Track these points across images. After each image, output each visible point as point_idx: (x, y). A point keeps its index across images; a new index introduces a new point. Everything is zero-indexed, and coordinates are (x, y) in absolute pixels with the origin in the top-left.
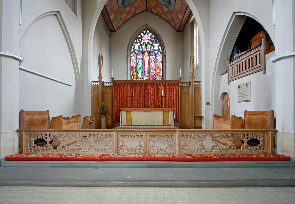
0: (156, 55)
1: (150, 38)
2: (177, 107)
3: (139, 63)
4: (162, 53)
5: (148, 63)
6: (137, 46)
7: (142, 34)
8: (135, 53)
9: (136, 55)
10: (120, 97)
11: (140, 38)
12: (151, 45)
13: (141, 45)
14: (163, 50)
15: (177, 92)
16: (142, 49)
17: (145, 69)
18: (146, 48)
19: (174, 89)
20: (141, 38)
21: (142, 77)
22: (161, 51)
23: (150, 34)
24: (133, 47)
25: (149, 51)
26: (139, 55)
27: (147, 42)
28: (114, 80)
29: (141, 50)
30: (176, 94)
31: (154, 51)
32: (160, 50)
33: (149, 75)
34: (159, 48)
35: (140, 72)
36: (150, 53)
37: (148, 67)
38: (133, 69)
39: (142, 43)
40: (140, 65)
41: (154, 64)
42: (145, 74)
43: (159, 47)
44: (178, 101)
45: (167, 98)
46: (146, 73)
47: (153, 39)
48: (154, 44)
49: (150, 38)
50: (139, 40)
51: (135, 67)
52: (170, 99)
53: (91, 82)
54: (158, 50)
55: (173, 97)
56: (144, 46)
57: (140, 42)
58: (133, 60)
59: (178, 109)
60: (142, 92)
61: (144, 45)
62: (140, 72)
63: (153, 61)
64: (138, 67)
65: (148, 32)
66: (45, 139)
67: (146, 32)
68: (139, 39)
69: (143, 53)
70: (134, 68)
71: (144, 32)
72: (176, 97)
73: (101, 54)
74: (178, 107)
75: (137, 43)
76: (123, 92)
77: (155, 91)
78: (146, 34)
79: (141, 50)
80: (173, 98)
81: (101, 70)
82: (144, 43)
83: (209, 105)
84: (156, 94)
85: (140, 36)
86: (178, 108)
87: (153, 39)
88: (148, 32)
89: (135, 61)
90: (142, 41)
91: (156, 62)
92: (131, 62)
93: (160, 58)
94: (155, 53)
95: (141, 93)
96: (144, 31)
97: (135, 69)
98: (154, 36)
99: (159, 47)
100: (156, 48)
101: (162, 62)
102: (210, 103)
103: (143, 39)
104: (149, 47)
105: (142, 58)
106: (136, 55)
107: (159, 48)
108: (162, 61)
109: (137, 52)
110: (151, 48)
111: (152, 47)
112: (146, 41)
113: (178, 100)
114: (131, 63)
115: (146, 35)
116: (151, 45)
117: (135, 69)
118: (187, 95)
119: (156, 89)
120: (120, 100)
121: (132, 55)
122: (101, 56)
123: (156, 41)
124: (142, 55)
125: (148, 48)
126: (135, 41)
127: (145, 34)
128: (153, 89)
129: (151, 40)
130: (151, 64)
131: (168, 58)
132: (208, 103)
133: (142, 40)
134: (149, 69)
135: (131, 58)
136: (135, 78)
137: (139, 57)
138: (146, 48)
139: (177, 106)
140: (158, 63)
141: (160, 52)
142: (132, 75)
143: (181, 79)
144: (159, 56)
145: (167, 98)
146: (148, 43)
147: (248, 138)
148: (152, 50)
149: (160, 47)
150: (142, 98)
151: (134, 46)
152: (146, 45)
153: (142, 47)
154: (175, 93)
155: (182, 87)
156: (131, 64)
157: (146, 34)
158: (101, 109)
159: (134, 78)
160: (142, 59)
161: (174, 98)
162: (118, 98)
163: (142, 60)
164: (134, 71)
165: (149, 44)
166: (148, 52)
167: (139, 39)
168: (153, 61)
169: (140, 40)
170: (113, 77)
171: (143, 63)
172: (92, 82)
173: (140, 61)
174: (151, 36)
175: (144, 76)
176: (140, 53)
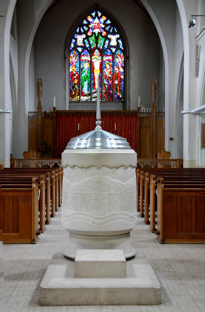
0: (113, 55)
1: (103, 26)
2: (135, 144)
3: (84, 68)
4: (123, 52)
5: (100, 68)
6: (80, 39)
7: (90, 19)
8: (77, 51)
9: (80, 54)
10: (64, 131)
11: (85, 25)
12: (106, 38)
13: (87, 37)
14: (126, 47)
15: (135, 126)
16: (89, 44)
17: (94, 79)
18: (97, 43)
19: (131, 120)
20: (87, 25)
21: (89, 92)
22: (122, 48)
23: (104, 18)
24: (74, 41)
25: (101, 48)
26: (83, 55)
27: (99, 32)
28: (56, 109)
29: (88, 46)
30: (134, 127)
31: (110, 47)
32: (121, 47)
33: (102, 90)
34: (118, 43)
35: (86, 84)
36: (102, 52)
37: (100, 76)
38: (74, 79)
39: (89, 34)
40: (86, 71)
41: (109, 71)
42: (94, 88)
43: (119, 41)
44: (136, 135)
45: (123, 133)
46: (97, 86)
47: (109, 27)
48: (109, 36)
49: (103, 26)
50: (83, 29)
51: (77, 75)
52: (126, 134)
53: (28, 113)
54: (117, 47)
55: (131, 131)
56: (92, 40)
57: (86, 32)
58: (74, 64)
59: (136, 145)
60: (91, 124)
61: (93, 38)
62: (86, 84)
63: (108, 66)
64: (83, 75)
65: (100, 14)
66: (49, 165)
67: (97, 15)
68: (85, 27)
69: (91, 52)
70: (75, 77)
71: (94, 14)
72: (134, 131)
73: (41, 79)
74: (137, 143)
75: (80, 33)
76: (67, 124)
77: (107, 123)
78: (97, 18)
79: (88, 46)
80: (131, 133)
81: (41, 98)
82: (93, 33)
83: (173, 141)
84: (109, 127)
85: (85, 22)
86: (137, 144)
87: (109, 27)
88: (100, 14)
89: (78, 66)
90: (88, 30)
91: (113, 66)
92: (70, 67)
93: (120, 60)
94: (111, 51)
95: (90, 126)
96: (93, 12)
97: (77, 78)
98: (110, 22)
99: (119, 41)
100: (113, 43)
101: (124, 68)
102: (174, 138)
103: (90, 26)
104: (101, 41)
105: (90, 60)
106: (80, 54)
107: (118, 43)
108: (123, 65)
109: (80, 50)
110: (104, 43)
111: (107, 42)
112: (97, 31)
113: (137, 134)
114: (71, 68)
115: (97, 20)
116: (106, 38)
117: (77, 78)
118: (148, 129)
119: (109, 122)
120: (64, 135)
121: (72, 55)
122: (40, 81)
123: (113, 30)
124: (89, 54)
125: (99, 42)
126: (78, 30)
127: (94, 18)
128: (105, 121)
129: (104, 29)
130: (105, 70)
131: (133, 62)
132: (171, 139)
133: (89, 28)
134: (101, 78)
135: (71, 59)
136: (77, 95)
137: (83, 58)
138: (97, 43)
139: (135, 142)
140: (117, 69)
141: (121, 49)
142: (72, 89)
143: (139, 109)
144: (119, 57)
145: (123, 133)
146: (100, 33)
147: (144, 164)
148: (106, 46)
149: (120, 41)
150: (91, 121)
151: (76, 39)
152: (97, 38)
153: (89, 42)
154: (133, 126)
155: (142, 119)
156: (71, 70)
157: (97, 18)
158: (44, 146)
159: (75, 93)
160: (88, 61)
161: (132, 132)
162: (61, 132)
163: (90, 64)
164: (76, 81)
165: (102, 36)
166: (99, 49)
167: (85, 27)
168: (108, 66)
169: (86, 28)
170: (55, 106)
171: (92, 68)
172: (29, 113)
173: (86, 66)
174: (105, 21)
175: (93, 91)
176: (86, 51)
